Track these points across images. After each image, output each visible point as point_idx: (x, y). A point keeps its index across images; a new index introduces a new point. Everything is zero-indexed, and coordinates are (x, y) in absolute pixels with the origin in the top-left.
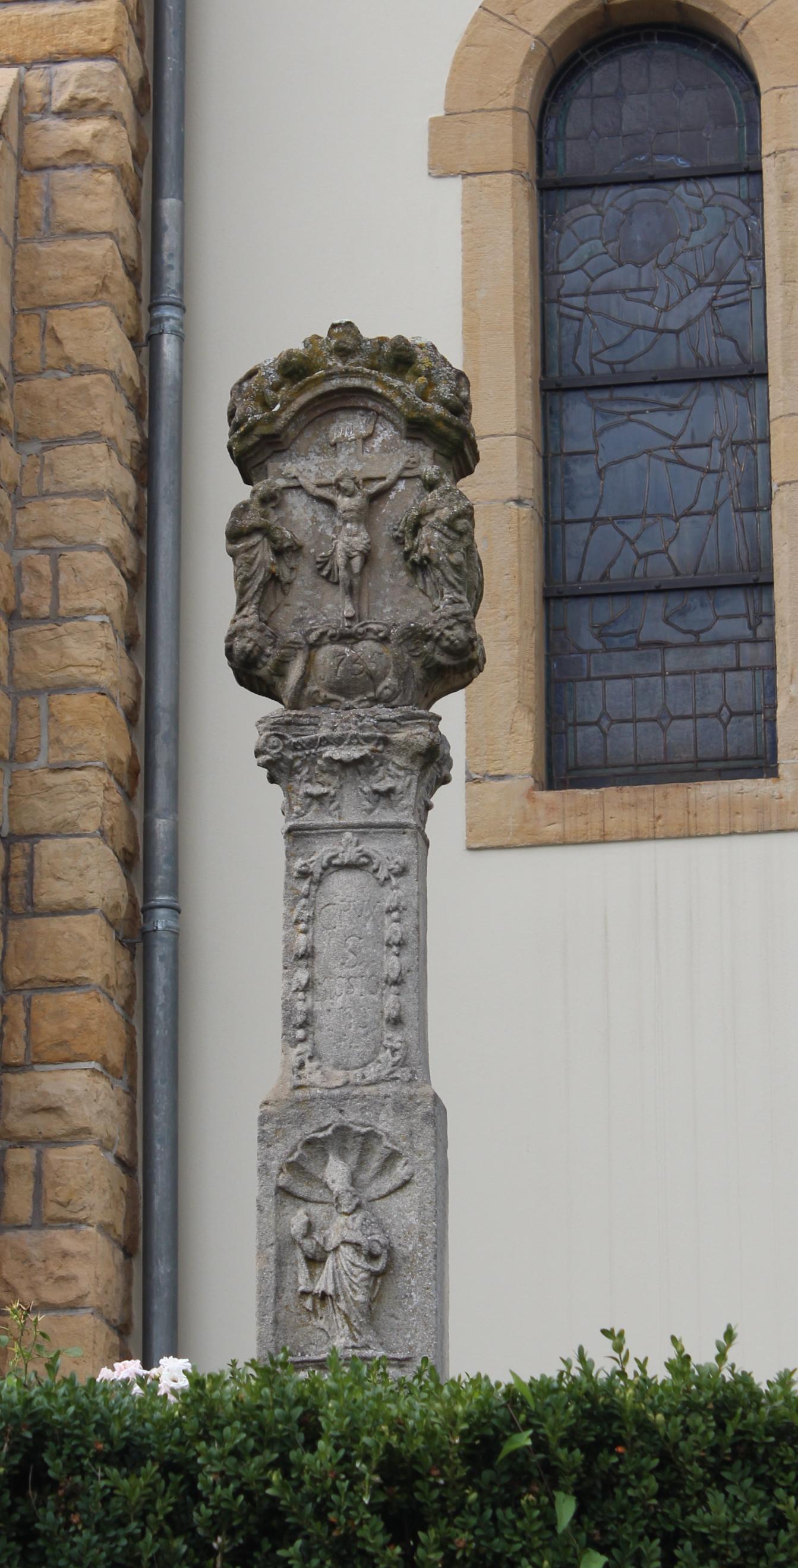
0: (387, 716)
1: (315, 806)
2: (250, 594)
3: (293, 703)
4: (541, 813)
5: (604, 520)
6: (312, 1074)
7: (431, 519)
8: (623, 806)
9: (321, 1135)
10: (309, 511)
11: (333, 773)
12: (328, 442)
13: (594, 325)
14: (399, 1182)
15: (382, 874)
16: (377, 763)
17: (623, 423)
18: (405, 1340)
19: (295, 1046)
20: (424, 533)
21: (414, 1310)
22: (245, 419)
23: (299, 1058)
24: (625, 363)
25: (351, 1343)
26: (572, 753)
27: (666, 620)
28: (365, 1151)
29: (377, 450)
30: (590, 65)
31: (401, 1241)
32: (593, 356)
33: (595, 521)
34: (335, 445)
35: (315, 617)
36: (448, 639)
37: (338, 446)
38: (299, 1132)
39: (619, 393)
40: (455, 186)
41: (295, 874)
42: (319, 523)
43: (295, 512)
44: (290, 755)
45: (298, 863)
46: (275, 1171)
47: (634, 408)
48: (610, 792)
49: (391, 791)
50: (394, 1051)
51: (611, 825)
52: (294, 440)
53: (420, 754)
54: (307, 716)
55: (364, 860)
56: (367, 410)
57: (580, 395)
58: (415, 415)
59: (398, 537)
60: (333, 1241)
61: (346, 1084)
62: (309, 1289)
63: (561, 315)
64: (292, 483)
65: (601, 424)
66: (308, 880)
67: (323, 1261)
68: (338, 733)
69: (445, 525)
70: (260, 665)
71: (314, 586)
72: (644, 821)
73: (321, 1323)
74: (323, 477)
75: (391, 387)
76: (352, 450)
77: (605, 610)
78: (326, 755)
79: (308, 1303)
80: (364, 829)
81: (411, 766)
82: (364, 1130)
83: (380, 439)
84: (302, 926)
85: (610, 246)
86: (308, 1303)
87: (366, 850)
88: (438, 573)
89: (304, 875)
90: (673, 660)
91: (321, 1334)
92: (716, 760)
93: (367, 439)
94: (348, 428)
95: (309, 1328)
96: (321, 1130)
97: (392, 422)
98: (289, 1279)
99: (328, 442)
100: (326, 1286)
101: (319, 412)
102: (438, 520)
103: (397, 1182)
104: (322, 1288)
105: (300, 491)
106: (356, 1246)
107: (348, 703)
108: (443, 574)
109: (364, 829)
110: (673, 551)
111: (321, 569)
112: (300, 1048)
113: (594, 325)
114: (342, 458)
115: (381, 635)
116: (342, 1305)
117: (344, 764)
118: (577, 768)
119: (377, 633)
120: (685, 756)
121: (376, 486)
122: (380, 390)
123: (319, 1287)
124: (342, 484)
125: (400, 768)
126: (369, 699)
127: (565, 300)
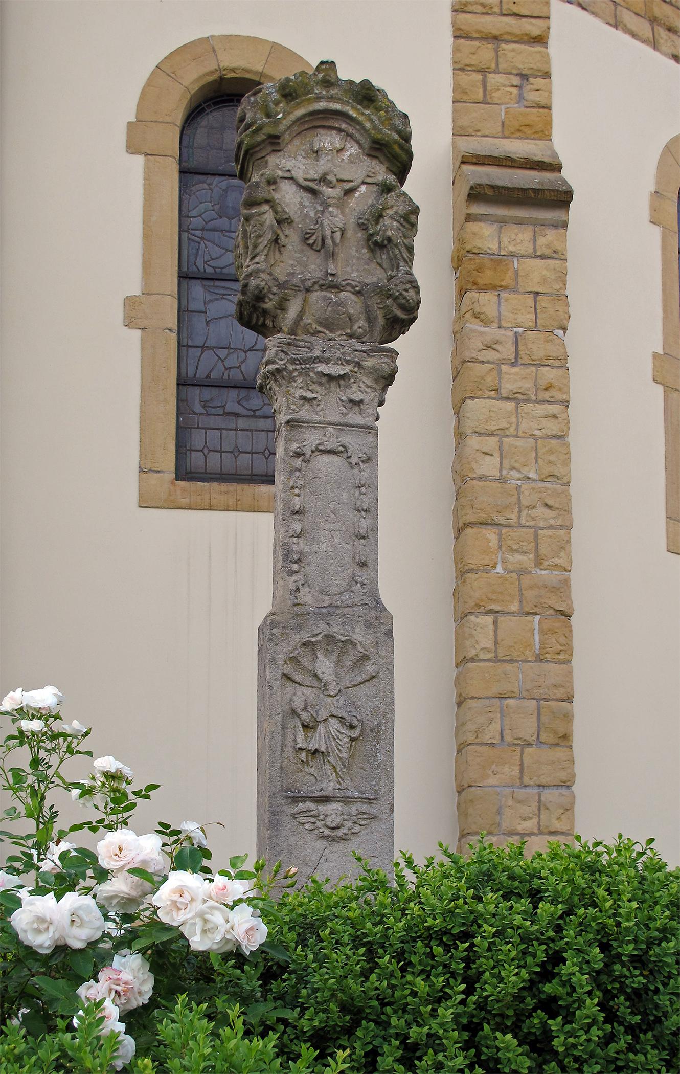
0: (360, 348)
1: (307, 406)
2: (261, 247)
3: (292, 330)
4: (179, 492)
5: (209, 348)
6: (306, 596)
7: (390, 212)
8: (221, 493)
9: (313, 639)
10: (298, 197)
11: (321, 384)
12: (312, 150)
13: (206, 247)
14: (368, 677)
15: (354, 460)
16: (352, 381)
17: (218, 299)
18: (371, 785)
19: (291, 576)
20: (387, 221)
21: (379, 765)
22: (255, 122)
23: (295, 584)
24: (222, 268)
25: (338, 786)
26: (188, 464)
27: (239, 402)
28: (343, 653)
29: (346, 161)
30: (208, 111)
31: (369, 718)
32: (205, 262)
33: (203, 348)
34: (317, 152)
35: (302, 273)
36: (405, 298)
37: (320, 153)
38: (298, 636)
39: (218, 283)
40: (140, 160)
41: (291, 454)
42: (305, 207)
43: (287, 196)
44: (291, 367)
45: (294, 446)
46: (281, 663)
47: (226, 292)
48: (215, 485)
49: (362, 401)
50: (363, 584)
51: (214, 501)
52: (287, 144)
53: (383, 378)
54: (303, 340)
55: (341, 448)
56: (340, 130)
57: (199, 281)
58: (379, 136)
59: (363, 224)
60: (323, 714)
61: (331, 605)
62: (304, 746)
63: (189, 239)
64: (286, 175)
65: (208, 297)
66: (301, 459)
67: (314, 728)
68: (327, 355)
69: (402, 217)
70: (267, 300)
71: (302, 251)
72: (231, 501)
73: (312, 771)
74: (308, 173)
75: (363, 114)
76: (330, 157)
77: (207, 393)
78: (319, 369)
79: (303, 756)
80: (342, 426)
81: (375, 386)
82: (344, 639)
83: (348, 153)
84: (296, 491)
85: (216, 207)
86: (303, 756)
87: (343, 442)
88: (397, 251)
89: (298, 454)
90: (242, 423)
91: (312, 777)
92: (261, 476)
93: (340, 151)
94: (328, 140)
95: (303, 773)
96: (313, 636)
97: (358, 142)
98: (290, 738)
99: (312, 150)
100: (319, 745)
101: (306, 126)
102: (396, 213)
103: (365, 677)
104: (317, 746)
105: (291, 182)
106: (341, 719)
107: (331, 335)
108: (401, 252)
109: (342, 426)
110: (243, 367)
111: (308, 239)
112: (294, 578)
113: (206, 247)
114: (322, 162)
115: (357, 289)
116: (331, 759)
117: (330, 378)
118: (191, 472)
119: (353, 287)
120: (246, 472)
121: (350, 185)
122: (355, 115)
123: (312, 746)
124: (328, 178)
125: (368, 387)
126: (346, 334)
127: (193, 232)
